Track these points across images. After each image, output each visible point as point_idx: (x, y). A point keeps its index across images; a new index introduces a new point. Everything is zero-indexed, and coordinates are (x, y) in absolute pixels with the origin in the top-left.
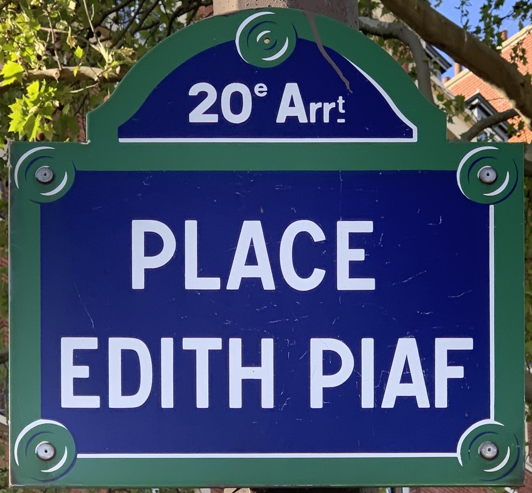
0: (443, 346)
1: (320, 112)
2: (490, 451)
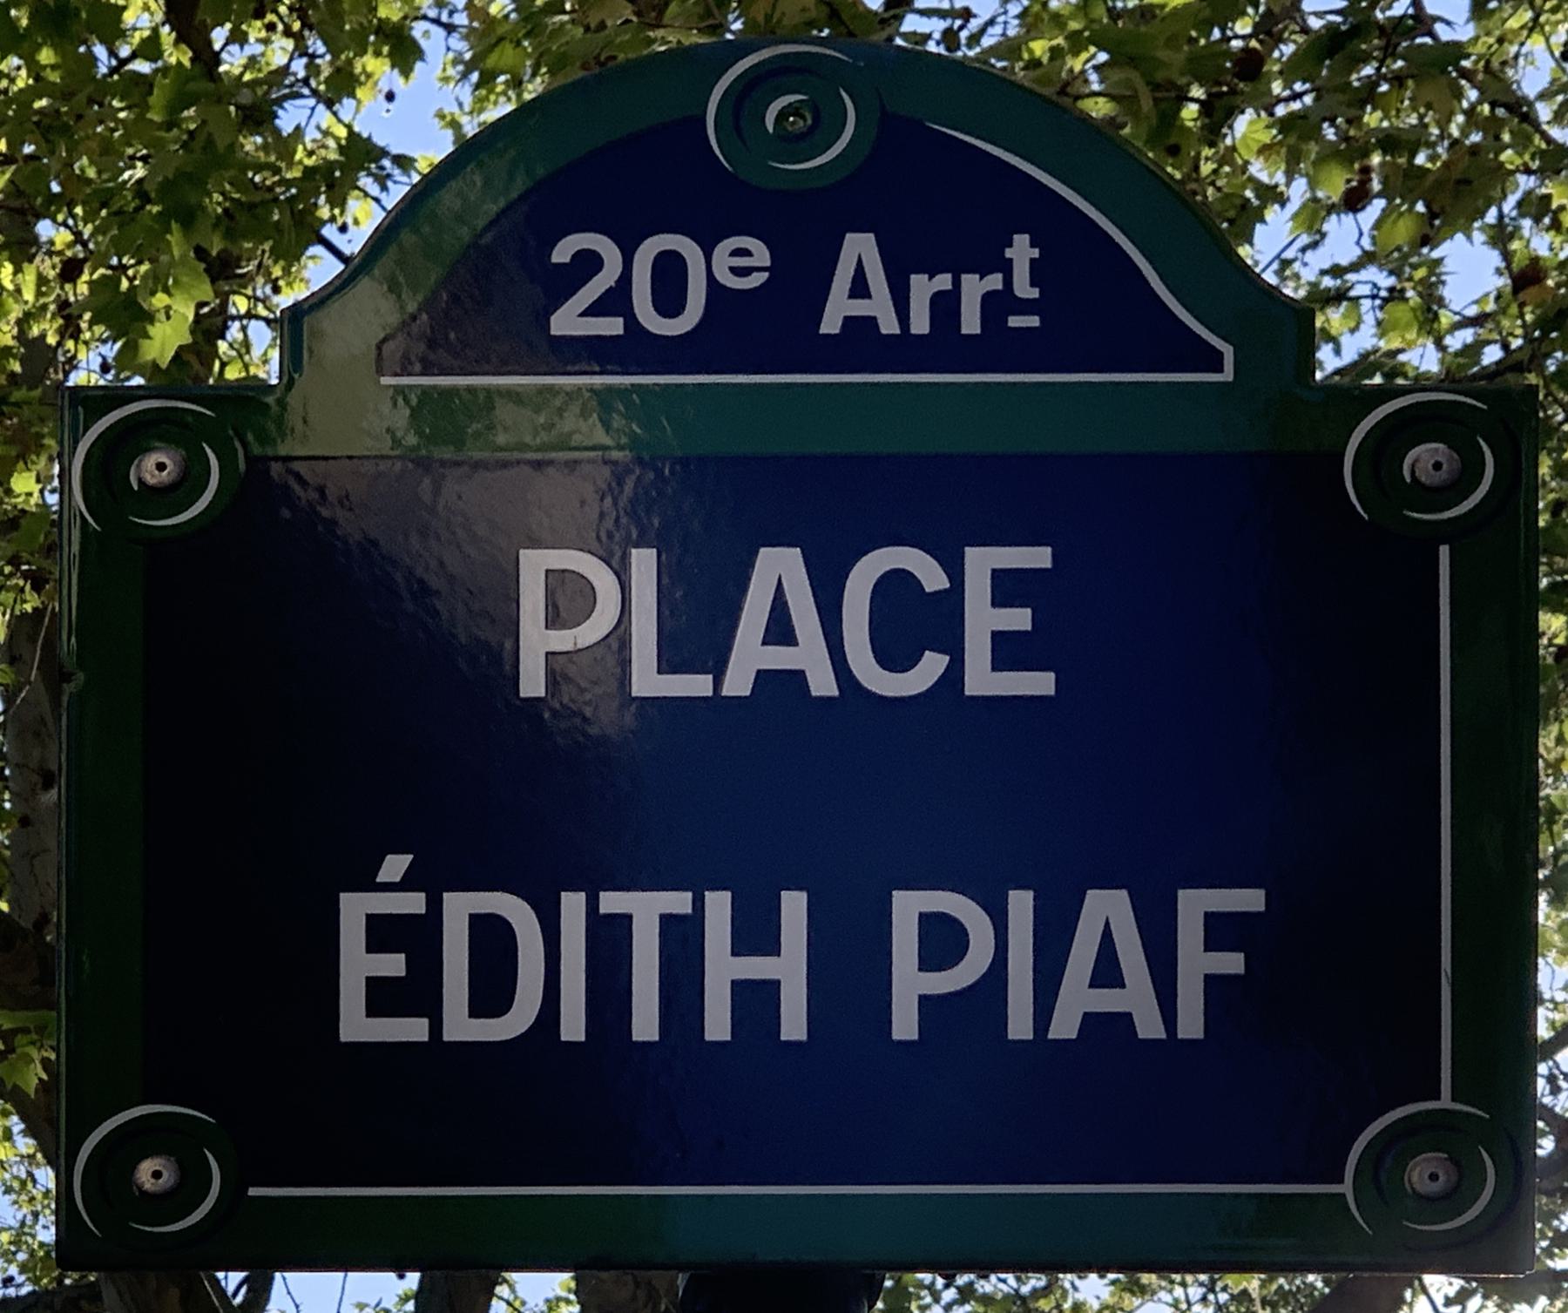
0: (1194, 906)
1: (946, 306)
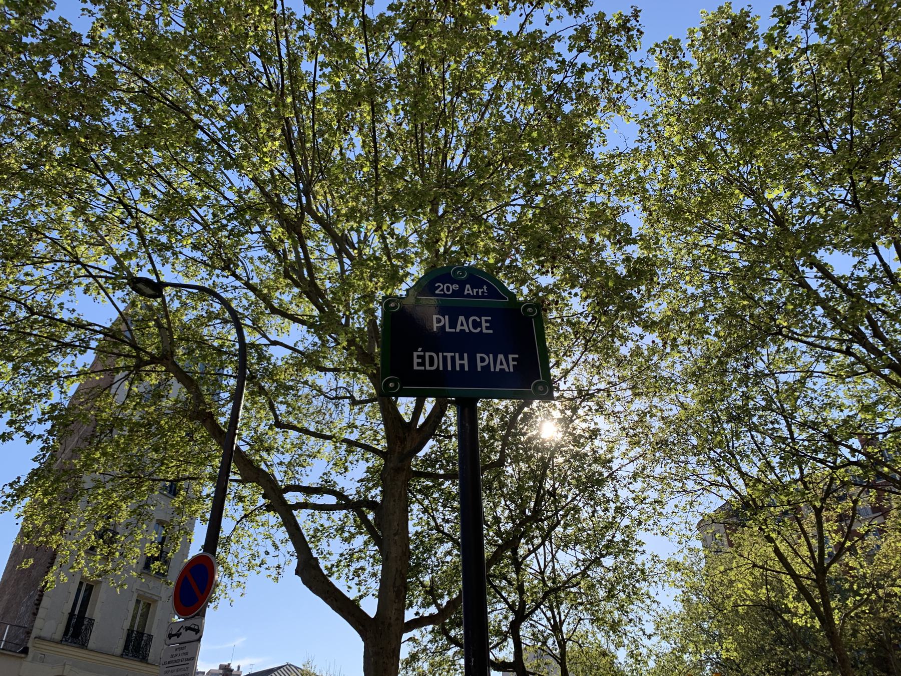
1: (477, 292)
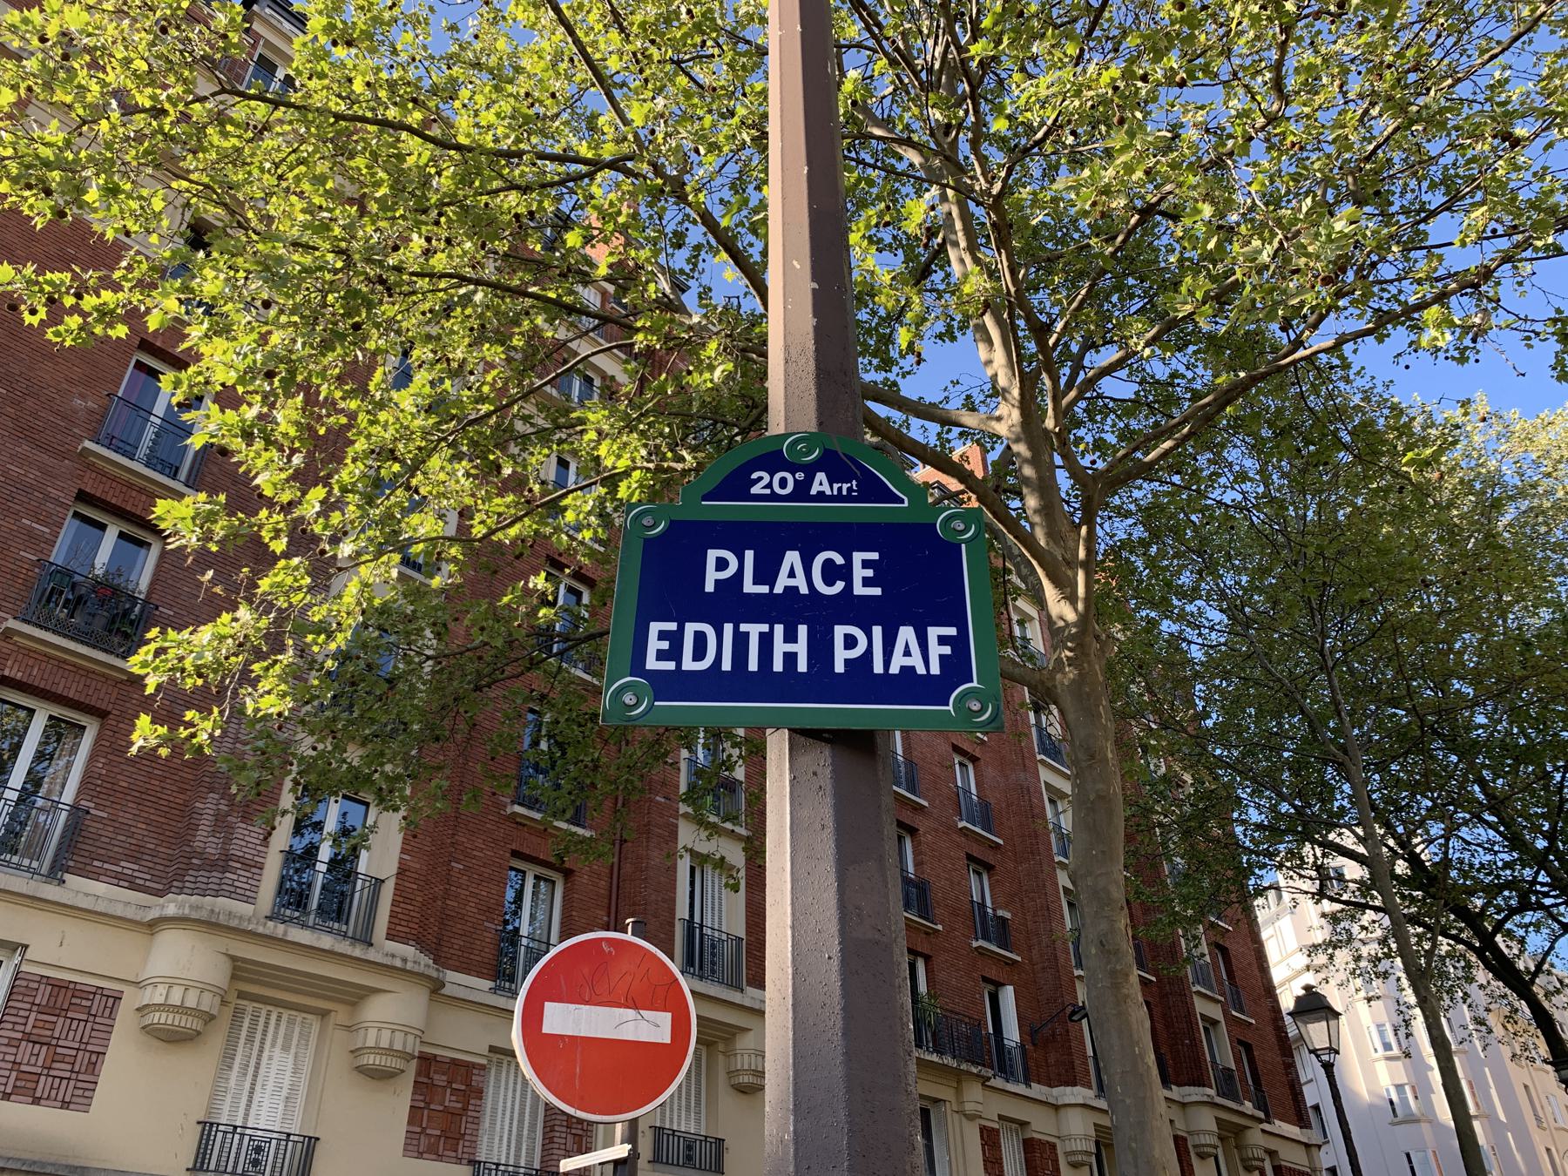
0: (933, 633)
1: (840, 489)
2: (975, 706)
